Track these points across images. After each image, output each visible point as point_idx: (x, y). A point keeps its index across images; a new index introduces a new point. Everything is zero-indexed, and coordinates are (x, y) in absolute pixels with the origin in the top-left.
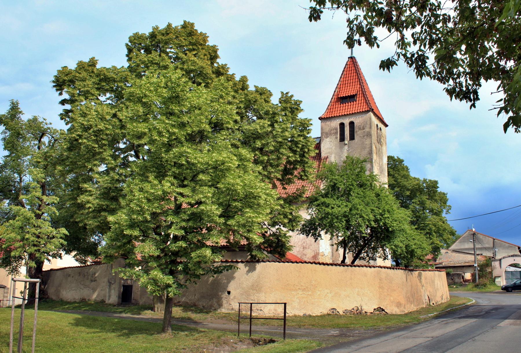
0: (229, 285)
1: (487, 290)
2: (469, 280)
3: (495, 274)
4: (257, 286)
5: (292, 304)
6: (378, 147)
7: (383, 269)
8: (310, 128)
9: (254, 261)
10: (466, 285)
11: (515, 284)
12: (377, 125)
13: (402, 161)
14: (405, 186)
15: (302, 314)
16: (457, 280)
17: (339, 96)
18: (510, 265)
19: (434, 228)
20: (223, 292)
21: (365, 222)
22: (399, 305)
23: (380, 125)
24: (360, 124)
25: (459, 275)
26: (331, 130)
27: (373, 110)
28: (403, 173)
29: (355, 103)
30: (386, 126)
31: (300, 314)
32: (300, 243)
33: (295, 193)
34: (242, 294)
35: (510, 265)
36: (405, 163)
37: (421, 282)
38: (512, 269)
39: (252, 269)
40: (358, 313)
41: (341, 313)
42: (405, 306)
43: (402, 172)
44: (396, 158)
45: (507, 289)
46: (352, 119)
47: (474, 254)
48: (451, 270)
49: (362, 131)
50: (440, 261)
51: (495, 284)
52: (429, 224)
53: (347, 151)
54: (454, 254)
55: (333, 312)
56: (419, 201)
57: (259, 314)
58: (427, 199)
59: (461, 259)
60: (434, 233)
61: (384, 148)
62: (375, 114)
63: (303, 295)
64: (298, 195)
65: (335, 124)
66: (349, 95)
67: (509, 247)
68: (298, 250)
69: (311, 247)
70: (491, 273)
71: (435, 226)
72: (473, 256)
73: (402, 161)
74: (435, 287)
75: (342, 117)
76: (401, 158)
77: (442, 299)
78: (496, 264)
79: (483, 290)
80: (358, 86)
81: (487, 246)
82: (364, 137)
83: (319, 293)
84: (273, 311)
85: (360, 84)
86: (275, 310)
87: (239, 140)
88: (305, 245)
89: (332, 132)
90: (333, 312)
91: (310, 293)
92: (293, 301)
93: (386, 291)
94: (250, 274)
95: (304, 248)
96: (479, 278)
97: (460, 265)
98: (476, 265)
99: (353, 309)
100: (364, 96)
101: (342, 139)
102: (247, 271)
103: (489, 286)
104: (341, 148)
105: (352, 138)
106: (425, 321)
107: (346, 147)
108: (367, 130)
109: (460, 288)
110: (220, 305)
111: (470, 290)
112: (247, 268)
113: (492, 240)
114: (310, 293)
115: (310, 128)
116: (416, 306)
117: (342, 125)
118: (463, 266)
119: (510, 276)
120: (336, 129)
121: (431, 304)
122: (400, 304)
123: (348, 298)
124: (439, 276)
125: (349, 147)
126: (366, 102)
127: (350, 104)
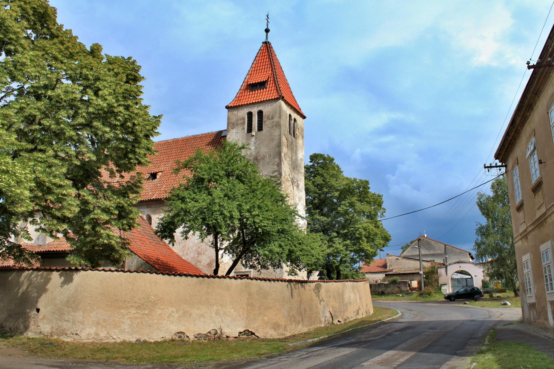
0: (40, 300)
1: (432, 299)
2: (416, 288)
3: (441, 281)
4: (74, 302)
5: (120, 326)
6: (290, 139)
7: (254, 281)
8: (140, 97)
9: (69, 272)
10: (411, 293)
11: (457, 292)
12: (290, 116)
13: (333, 160)
14: (333, 185)
15: (134, 340)
16: (403, 288)
17: (249, 83)
18: (456, 272)
19: (364, 233)
20: (31, 309)
21: (226, 221)
22: (276, 326)
23: (294, 115)
24: (269, 113)
25: (405, 283)
26: (238, 120)
27: (283, 97)
28: (332, 172)
29: (265, 90)
30: (304, 117)
31: (131, 340)
32: (194, 248)
33: (129, 181)
34: (54, 313)
35: (456, 272)
36: (336, 162)
37: (318, 296)
38: (459, 276)
39: (68, 280)
40: (216, 339)
41: (192, 338)
42: (285, 327)
43: (331, 171)
44: (326, 156)
45: (450, 298)
46: (261, 108)
47: (419, 260)
48: (398, 278)
49: (271, 121)
50: (391, 268)
51: (441, 292)
52: (359, 228)
53: (255, 143)
54: (405, 261)
55: (180, 337)
56: (349, 203)
57: (75, 339)
58: (356, 200)
59: (411, 266)
60: (364, 238)
61: (300, 141)
62: (286, 103)
63: (136, 315)
64: (133, 184)
65: (243, 113)
66: (259, 81)
67: (461, 253)
68: (192, 256)
69: (207, 253)
70: (437, 280)
71: (365, 230)
72: (418, 262)
73: (333, 160)
74: (353, 300)
75: (250, 106)
76: (331, 157)
77: (358, 313)
78: (442, 271)
79: (428, 299)
80: (270, 72)
81: (439, 252)
82: (272, 127)
83: (160, 312)
84: (93, 336)
85: (272, 70)
86: (97, 334)
87: (39, 109)
88: (199, 250)
89: (239, 122)
90: (180, 337)
91: (146, 312)
92: (123, 323)
93: (257, 308)
94: (65, 286)
95: (199, 254)
96: (425, 286)
97: (411, 272)
98: (421, 272)
99: (209, 332)
100: (275, 83)
101: (250, 130)
102: (62, 283)
103: (434, 295)
104: (248, 139)
105: (260, 128)
106: (295, 350)
107: (253, 139)
108: (276, 119)
109: (406, 297)
110: (26, 328)
111: (414, 299)
112: (63, 278)
113: (443, 246)
114: (146, 312)
115: (140, 97)
116: (306, 326)
117: (250, 115)
118: (413, 274)
119: (456, 283)
120: (244, 119)
121: (336, 322)
122: (279, 326)
123: (202, 319)
124: (353, 288)
125: (256, 139)
126: (277, 89)
127: (259, 91)
